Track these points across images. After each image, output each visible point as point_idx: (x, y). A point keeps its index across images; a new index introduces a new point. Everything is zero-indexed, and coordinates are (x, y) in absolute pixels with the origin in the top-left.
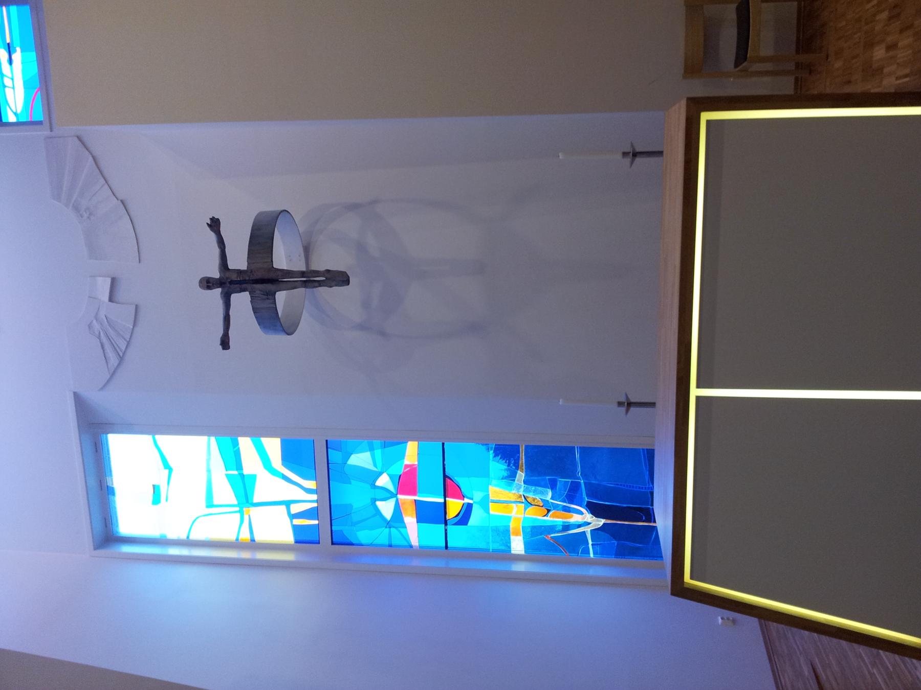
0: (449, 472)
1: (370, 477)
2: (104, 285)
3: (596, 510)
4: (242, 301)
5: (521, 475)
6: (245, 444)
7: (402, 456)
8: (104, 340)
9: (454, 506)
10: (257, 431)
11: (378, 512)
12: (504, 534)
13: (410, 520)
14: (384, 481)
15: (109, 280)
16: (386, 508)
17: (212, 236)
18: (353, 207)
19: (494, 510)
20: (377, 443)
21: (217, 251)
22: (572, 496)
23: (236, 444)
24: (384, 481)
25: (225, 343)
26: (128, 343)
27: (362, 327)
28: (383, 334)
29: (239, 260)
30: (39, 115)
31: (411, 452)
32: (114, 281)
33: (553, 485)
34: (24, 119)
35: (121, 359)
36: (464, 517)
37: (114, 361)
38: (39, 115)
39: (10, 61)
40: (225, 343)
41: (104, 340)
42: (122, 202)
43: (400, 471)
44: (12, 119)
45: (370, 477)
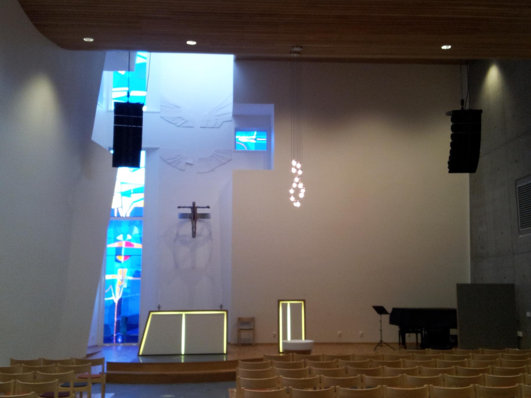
0: (132, 257)
1: (130, 232)
2: (190, 161)
3: (120, 301)
4: (189, 211)
5: (131, 278)
6: (142, 196)
7: (137, 242)
8: (175, 159)
9: (121, 258)
10: (146, 199)
11: (118, 234)
12: (112, 273)
13: (116, 245)
14: (129, 237)
15: (192, 163)
16: (120, 237)
17: (206, 206)
18: (210, 234)
19: (120, 270)
20: (142, 236)
21: (202, 206)
22: (124, 293)
23: (141, 192)
24: (129, 237)
25: (179, 207)
26: (174, 166)
27: (177, 235)
28: (175, 240)
29: (199, 211)
30: (238, 149)
31: (138, 246)
32: (191, 165)
33: (128, 288)
34: (237, 140)
35: (169, 164)
36: (117, 261)
37: (169, 161)
38: (238, 149)
39: (252, 139)
40: (179, 207)
41: (175, 159)
42: (213, 170)
43: (132, 243)
44: (237, 137)
45: (130, 232)
